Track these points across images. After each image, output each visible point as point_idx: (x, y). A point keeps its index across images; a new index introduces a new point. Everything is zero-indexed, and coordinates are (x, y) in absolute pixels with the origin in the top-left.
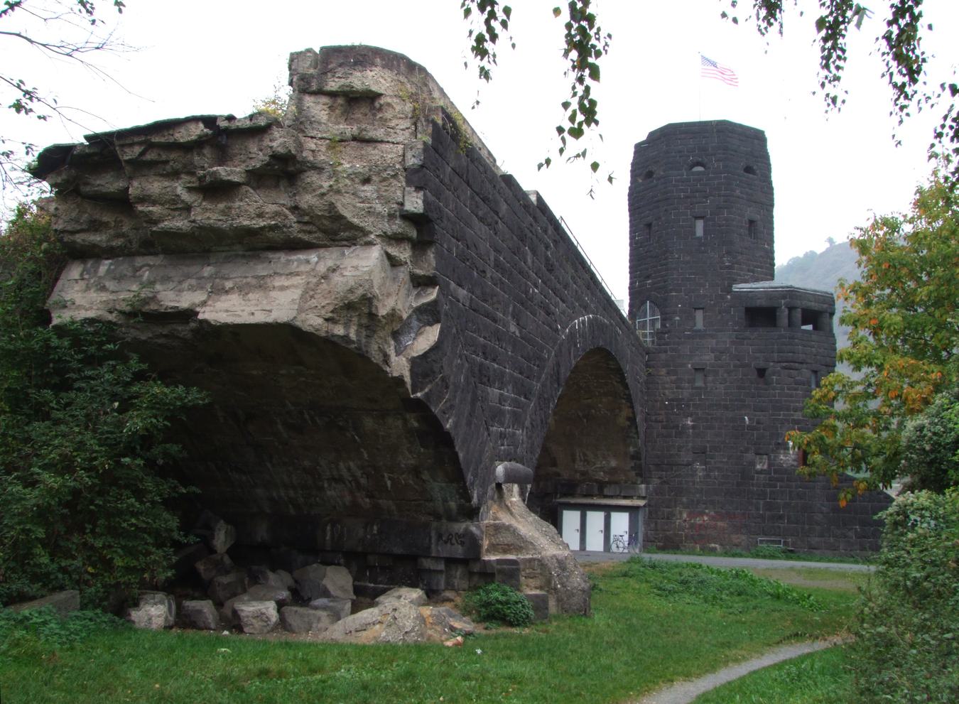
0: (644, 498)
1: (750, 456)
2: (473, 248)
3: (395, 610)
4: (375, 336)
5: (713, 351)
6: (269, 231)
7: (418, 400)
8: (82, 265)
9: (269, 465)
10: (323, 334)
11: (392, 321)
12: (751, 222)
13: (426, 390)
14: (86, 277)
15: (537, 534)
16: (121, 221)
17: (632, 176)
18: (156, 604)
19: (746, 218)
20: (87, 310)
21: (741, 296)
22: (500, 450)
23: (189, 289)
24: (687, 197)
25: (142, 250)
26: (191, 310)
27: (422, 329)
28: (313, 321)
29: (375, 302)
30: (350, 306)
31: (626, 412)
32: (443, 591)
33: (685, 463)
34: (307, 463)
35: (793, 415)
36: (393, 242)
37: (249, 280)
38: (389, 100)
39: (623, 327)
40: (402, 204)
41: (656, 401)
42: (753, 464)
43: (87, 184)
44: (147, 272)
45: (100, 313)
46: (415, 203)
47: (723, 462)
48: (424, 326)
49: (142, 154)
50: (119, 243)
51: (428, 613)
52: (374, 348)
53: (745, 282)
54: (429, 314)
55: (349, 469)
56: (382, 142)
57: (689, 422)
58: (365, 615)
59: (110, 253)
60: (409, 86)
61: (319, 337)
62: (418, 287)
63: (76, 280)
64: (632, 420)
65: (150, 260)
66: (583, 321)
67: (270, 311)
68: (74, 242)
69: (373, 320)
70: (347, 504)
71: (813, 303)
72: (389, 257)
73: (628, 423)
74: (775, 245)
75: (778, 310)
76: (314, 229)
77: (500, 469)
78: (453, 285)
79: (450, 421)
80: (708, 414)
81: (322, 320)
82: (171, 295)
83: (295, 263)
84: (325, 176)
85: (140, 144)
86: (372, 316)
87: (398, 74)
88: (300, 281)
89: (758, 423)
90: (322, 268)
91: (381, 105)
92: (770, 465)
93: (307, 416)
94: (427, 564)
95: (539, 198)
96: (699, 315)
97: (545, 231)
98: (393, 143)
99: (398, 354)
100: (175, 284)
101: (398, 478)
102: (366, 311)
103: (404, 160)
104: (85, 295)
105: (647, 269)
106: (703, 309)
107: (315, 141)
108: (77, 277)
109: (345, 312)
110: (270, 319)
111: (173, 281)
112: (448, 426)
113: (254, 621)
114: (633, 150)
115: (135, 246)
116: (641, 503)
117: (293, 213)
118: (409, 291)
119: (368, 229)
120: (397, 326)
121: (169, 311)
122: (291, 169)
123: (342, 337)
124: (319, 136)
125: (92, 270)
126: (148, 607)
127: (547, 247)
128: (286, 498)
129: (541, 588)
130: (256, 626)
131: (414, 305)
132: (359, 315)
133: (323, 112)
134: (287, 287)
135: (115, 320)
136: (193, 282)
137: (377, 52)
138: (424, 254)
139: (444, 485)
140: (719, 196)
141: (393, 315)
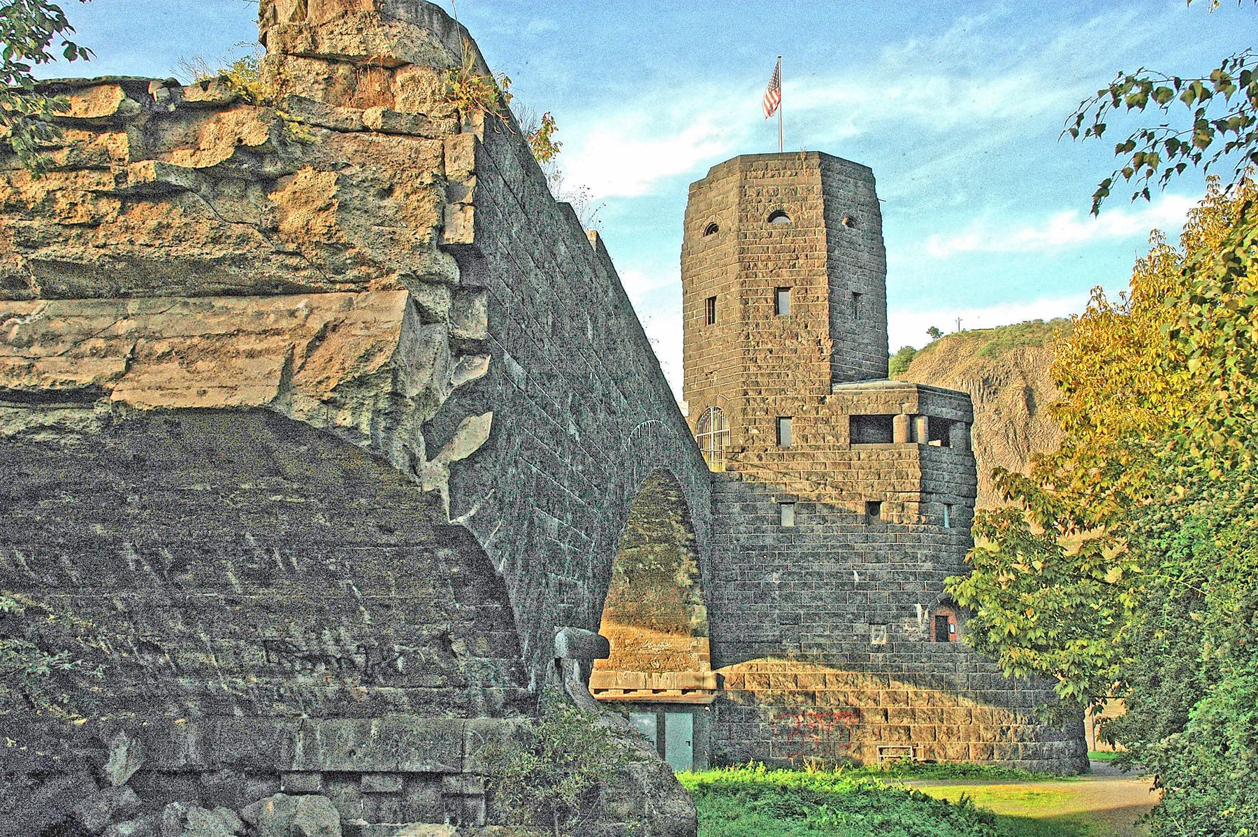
1: (860, 627)
13: (472, 512)
23: (93, 355)
29: (402, 376)
33: (770, 638)
34: (270, 633)
37: (195, 341)
42: (866, 637)
55: (337, 641)
75: (895, 419)
76: (304, 263)
77: (560, 639)
81: (318, 402)
83: (272, 316)
88: (283, 344)
92: (891, 638)
93: (277, 556)
99: (429, 460)
102: (388, 388)
112: (501, 569)
121: (58, 387)
132: (376, 395)
133: (316, 86)
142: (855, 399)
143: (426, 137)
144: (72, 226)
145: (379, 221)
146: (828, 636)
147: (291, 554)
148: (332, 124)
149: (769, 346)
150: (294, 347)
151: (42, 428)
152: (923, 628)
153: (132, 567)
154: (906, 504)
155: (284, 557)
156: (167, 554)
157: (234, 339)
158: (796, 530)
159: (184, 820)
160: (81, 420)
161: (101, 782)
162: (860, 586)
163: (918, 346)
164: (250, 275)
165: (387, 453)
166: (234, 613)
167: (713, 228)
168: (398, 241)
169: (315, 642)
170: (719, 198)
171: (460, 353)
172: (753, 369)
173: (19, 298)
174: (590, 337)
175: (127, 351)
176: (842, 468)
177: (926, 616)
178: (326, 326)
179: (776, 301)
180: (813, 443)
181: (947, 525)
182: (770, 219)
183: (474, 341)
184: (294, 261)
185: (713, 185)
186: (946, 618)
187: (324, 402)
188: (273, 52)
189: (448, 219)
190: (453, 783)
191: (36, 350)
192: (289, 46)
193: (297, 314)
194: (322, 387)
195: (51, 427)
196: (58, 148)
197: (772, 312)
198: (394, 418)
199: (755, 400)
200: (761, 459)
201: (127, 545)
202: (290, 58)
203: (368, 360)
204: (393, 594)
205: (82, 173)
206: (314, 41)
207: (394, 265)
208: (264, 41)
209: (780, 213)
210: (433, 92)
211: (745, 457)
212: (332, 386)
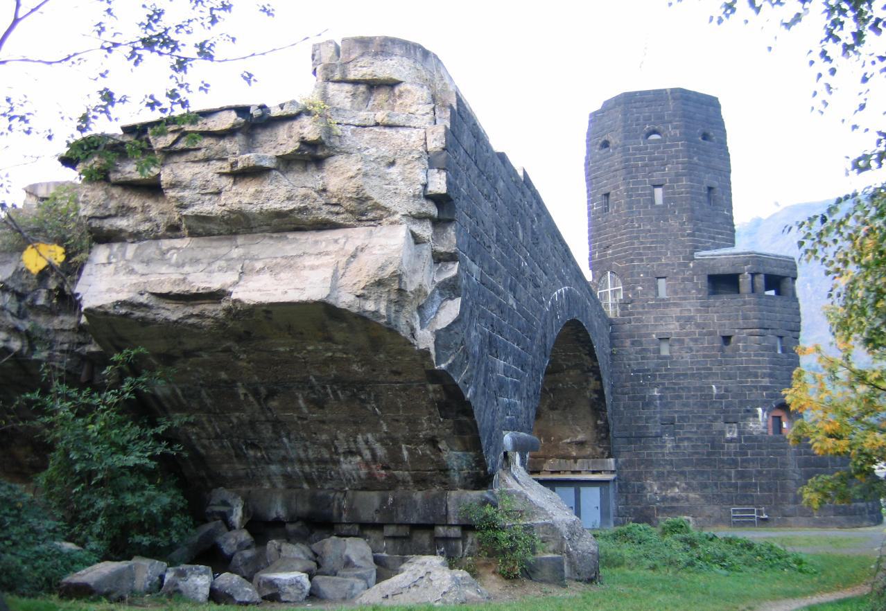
0: (613, 472)
1: (718, 425)
2: (481, 225)
4: (404, 311)
5: (678, 319)
7: (443, 371)
8: (108, 250)
9: (285, 440)
10: (356, 311)
11: (419, 296)
12: (710, 189)
14: (114, 260)
16: (148, 206)
17: (588, 146)
18: (201, 574)
19: (705, 186)
20: (118, 293)
21: (701, 264)
23: (220, 271)
24: (646, 165)
25: (168, 233)
26: (224, 291)
27: (444, 304)
28: (345, 299)
29: (404, 279)
30: (380, 283)
31: (593, 383)
33: (654, 435)
35: (760, 382)
38: (409, 87)
39: (591, 299)
40: (425, 186)
41: (622, 373)
42: (722, 433)
43: (117, 171)
44: (175, 255)
45: (131, 295)
46: (439, 184)
47: (692, 432)
48: (446, 300)
49: (175, 142)
50: (146, 228)
51: (460, 576)
52: (402, 321)
53: (707, 250)
54: (449, 289)
55: (367, 442)
56: (404, 126)
57: (656, 393)
59: (137, 236)
60: (424, 73)
61: (350, 313)
62: (438, 263)
63: (103, 264)
64: (600, 392)
65: (177, 243)
66: (561, 292)
68: (101, 228)
69: (401, 295)
70: (363, 476)
71: (775, 269)
72: (414, 235)
73: (596, 396)
74: (733, 211)
75: (741, 276)
76: (342, 210)
77: (508, 438)
78: (469, 260)
79: (470, 390)
80: (675, 384)
81: (354, 296)
82: (202, 276)
84: (353, 159)
85: (174, 132)
86: (401, 291)
89: (726, 390)
90: (350, 248)
91: (401, 92)
92: (740, 433)
93: (329, 391)
95: (525, 173)
96: (662, 283)
97: (531, 206)
98: (415, 127)
99: (422, 328)
100: (205, 266)
101: (415, 449)
102: (396, 287)
103: (426, 143)
104: (115, 277)
105: (607, 239)
106: (665, 277)
107: (340, 126)
108: (104, 261)
109: (375, 289)
110: (304, 298)
111: (202, 263)
112: (468, 396)
113: (290, 590)
114: (587, 119)
115: (162, 230)
116: (610, 477)
117: (321, 195)
119: (393, 209)
120: (422, 301)
121: (201, 291)
122: (320, 153)
123: (373, 312)
124: (345, 122)
125: (120, 254)
126: (194, 578)
127: (533, 221)
128: (300, 474)
129: (554, 552)
130: (293, 594)
131: (437, 280)
132: (389, 291)
133: (346, 99)
134: (318, 267)
135: (146, 302)
136: (222, 263)
137: (393, 41)
138: (444, 232)
139: (460, 453)
140: (677, 163)
141: (420, 291)
143: (415, 127)
144: (206, 194)
145: (387, 182)
146: (696, 432)
147: (338, 389)
148: (357, 123)
151: (192, 316)
152: (763, 424)
153: (242, 397)
155: (334, 392)
156: (263, 390)
158: (670, 357)
159: (280, 550)
160: (214, 311)
161: (230, 527)
165: (396, 326)
166: (302, 425)
167: (606, 144)
168: (399, 194)
173: (177, 237)
174: (521, 238)
175: (239, 267)
177: (765, 416)
178: (357, 249)
181: (779, 352)
184: (336, 209)
186: (780, 417)
189: (430, 179)
190: (441, 531)
191: (187, 269)
193: (339, 241)
194: (356, 287)
195: (197, 315)
196: (199, 149)
201: (239, 384)
203: (383, 270)
204: (401, 413)
205: (212, 162)
207: (398, 209)
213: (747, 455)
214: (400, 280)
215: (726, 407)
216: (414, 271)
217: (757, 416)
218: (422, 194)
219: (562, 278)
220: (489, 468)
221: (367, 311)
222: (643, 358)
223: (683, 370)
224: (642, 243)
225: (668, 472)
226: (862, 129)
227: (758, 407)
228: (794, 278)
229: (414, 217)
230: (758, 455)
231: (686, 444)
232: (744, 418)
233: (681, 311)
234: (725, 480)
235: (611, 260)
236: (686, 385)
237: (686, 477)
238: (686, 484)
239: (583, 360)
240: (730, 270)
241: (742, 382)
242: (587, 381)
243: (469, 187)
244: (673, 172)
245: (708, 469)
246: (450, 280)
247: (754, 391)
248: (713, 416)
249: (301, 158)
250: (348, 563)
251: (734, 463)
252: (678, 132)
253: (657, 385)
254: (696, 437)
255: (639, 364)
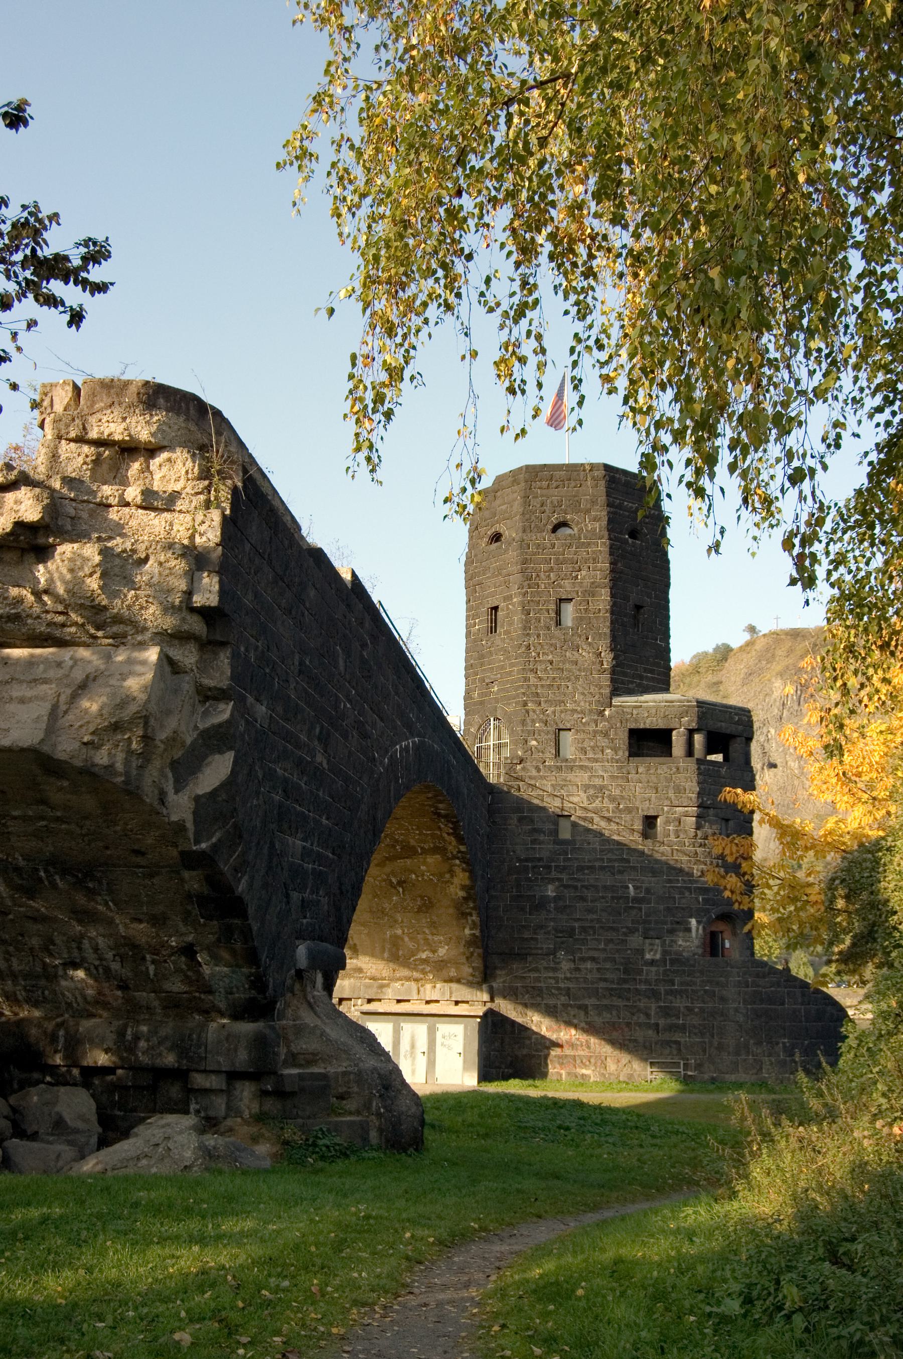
1: (635, 940)
3: (168, 1138)
4: (150, 767)
5: (586, 788)
6: (6, 622)
7: (203, 852)
15: (350, 1042)
22: (302, 924)
29: (152, 721)
32: (225, 1118)
36: (176, 642)
42: (640, 952)
58: (126, 1147)
62: (204, 702)
66: (407, 747)
67: (8, 730)
74: (671, 641)
75: (674, 733)
77: (302, 951)
78: (250, 699)
79: (243, 881)
87: (187, 420)
92: (665, 953)
94: (200, 1080)
97: (362, 624)
99: (177, 791)
112: (240, 889)
118: (194, 706)
131: (201, 726)
133: (85, 467)
134: (30, 700)
138: (215, 659)
142: (635, 712)
146: (605, 950)
147: (56, 873)
149: (550, 657)
150: (59, 695)
154: (683, 818)
157: (8, 686)
162: (636, 900)
163: (735, 644)
164: (24, 630)
165: (138, 788)
167: (497, 537)
169: (76, 951)
170: (504, 507)
171: (207, 698)
172: (533, 681)
174: (342, 668)
176: (620, 782)
178: (87, 677)
179: (558, 612)
180: (591, 755)
182: (555, 529)
183: (219, 689)
185: (498, 494)
187: (85, 744)
188: (49, 437)
192: (63, 432)
197: (553, 623)
198: (146, 756)
199: (534, 711)
200: (539, 770)
202: (63, 442)
203: (122, 708)
206: (84, 428)
208: (42, 426)
209: (563, 524)
210: (187, 472)
211: (523, 769)
212: (92, 729)
213: (673, 985)
214: (146, 724)
215: (647, 915)
216: (168, 712)
217: (689, 930)
218: (184, 605)
219: (409, 726)
220: (270, 991)
221: (97, 765)
222: (534, 841)
223: (589, 861)
224: (540, 679)
225: (563, 1005)
226: (754, 548)
227: (691, 917)
228: (749, 739)
229: (172, 636)
230: (688, 985)
231: (589, 965)
232: (671, 932)
233: (590, 778)
234: (642, 1019)
235: (497, 701)
236: (592, 882)
237: (587, 1013)
238: (587, 1023)
239: (444, 840)
240: (661, 725)
241: (670, 881)
242: (451, 872)
243: (256, 597)
244: (588, 581)
245: (620, 1003)
246: (220, 725)
247: (687, 894)
248: (627, 928)
249: (15, 544)
250: (59, 1125)
251: (655, 995)
252: (597, 525)
253: (552, 881)
254: (602, 956)
255: (527, 849)
